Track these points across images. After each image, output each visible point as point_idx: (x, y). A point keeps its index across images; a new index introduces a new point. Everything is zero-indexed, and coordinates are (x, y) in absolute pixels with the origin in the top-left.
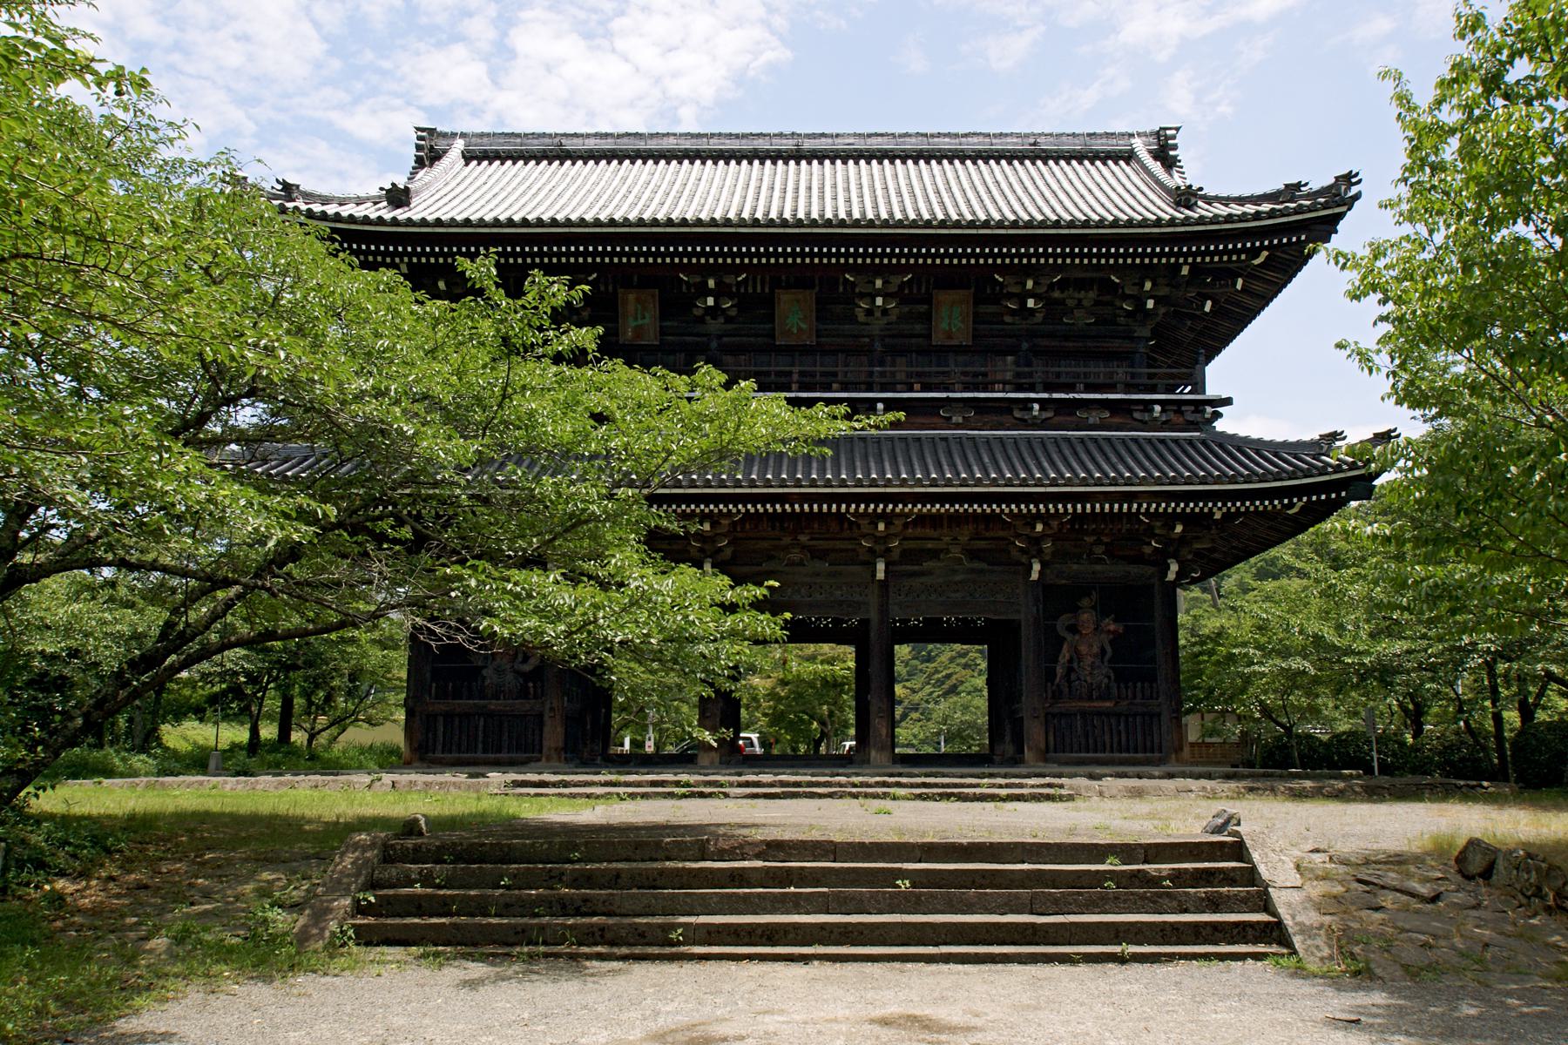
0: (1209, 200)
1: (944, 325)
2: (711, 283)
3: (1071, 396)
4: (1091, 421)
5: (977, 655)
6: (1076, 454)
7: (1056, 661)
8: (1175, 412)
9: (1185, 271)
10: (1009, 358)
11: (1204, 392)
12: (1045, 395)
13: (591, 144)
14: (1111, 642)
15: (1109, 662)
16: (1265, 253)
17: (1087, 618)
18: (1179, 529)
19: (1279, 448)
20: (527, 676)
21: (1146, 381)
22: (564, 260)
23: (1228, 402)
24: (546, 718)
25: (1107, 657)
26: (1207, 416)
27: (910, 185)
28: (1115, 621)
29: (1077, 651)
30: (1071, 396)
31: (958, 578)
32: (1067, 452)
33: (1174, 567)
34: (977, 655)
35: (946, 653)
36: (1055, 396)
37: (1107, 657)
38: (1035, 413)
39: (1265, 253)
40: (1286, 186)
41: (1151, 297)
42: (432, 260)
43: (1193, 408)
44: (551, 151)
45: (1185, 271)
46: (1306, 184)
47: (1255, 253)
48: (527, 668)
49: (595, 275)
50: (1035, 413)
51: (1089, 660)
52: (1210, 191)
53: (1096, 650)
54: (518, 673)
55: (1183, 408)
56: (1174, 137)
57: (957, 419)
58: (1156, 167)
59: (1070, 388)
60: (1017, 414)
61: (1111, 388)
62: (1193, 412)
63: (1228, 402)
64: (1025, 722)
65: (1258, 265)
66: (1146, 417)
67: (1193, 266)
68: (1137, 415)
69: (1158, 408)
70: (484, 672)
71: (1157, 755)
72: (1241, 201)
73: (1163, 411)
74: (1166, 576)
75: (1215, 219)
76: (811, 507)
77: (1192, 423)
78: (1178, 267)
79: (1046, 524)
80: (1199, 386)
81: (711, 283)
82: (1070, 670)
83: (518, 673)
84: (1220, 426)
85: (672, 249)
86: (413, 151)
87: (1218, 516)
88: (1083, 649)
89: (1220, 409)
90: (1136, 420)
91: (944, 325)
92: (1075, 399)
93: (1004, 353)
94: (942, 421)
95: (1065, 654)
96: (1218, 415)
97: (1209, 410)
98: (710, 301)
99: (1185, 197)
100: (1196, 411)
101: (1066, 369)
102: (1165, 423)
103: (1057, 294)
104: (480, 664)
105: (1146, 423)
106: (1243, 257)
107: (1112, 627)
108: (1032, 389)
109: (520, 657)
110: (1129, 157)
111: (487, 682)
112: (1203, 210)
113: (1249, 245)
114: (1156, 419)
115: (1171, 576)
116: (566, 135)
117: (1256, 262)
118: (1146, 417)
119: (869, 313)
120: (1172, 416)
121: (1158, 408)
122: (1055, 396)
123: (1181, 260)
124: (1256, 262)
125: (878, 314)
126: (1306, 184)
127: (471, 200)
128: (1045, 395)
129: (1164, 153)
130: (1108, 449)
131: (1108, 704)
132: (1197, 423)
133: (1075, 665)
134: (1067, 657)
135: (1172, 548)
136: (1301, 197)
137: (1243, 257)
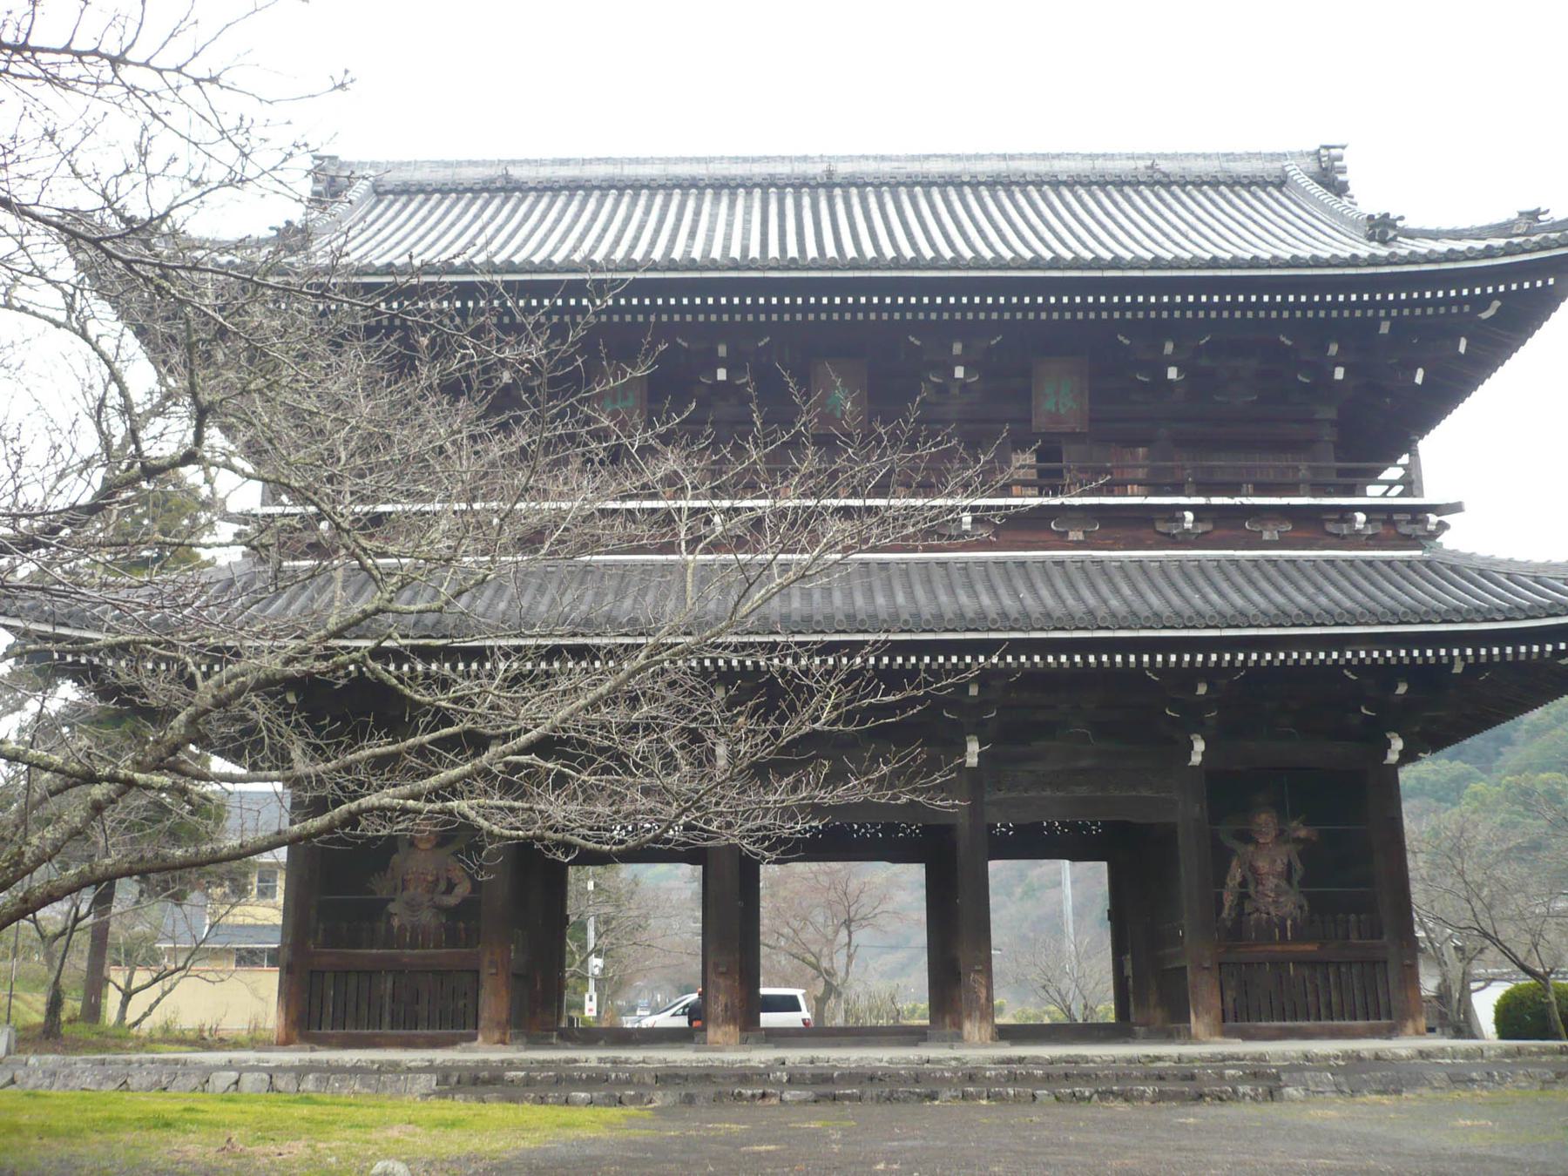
0: (1411, 234)
1: (1049, 405)
2: (722, 350)
3: (1237, 501)
4: (1266, 536)
5: (913, 875)
6: (1251, 582)
7: (1223, 884)
8: (1384, 522)
9: (1385, 328)
10: (1141, 450)
11: (1421, 495)
12: (1201, 500)
13: (546, 172)
14: (1300, 855)
15: (1303, 883)
16: (1497, 304)
17: (1265, 822)
18: (1402, 689)
19: (1513, 574)
20: (453, 913)
21: (1334, 479)
22: (823, 317)
23: (1456, 508)
24: (484, 976)
25: (1296, 878)
26: (1431, 527)
27: (1287, 208)
28: (1306, 824)
29: (1254, 870)
30: (1237, 501)
31: (1084, 763)
32: (1240, 580)
33: (1398, 744)
34: (913, 875)
35: (878, 873)
36: (1216, 501)
37: (1296, 878)
38: (1188, 525)
39: (1497, 304)
40: (1521, 214)
41: (1338, 365)
42: (640, 318)
43: (1409, 517)
44: (493, 181)
45: (1385, 328)
46: (1547, 211)
47: (1485, 301)
48: (451, 900)
49: (767, 340)
50: (1188, 525)
51: (1271, 882)
52: (1411, 223)
53: (1279, 867)
54: (441, 909)
55: (1395, 517)
56: (1340, 158)
57: (1076, 535)
58: (1328, 197)
59: (1233, 490)
60: (1161, 527)
61: (1293, 490)
62: (1409, 522)
63: (1456, 508)
64: (1190, 977)
65: (1485, 321)
66: (1345, 530)
67: (1396, 323)
68: (1330, 527)
69: (1361, 517)
70: (392, 908)
71: (1384, 1022)
72: (1457, 235)
73: (1196, 520)
74: (1385, 756)
75: (1412, 259)
76: (1085, 659)
77: (1408, 537)
78: (1376, 321)
79: (1211, 685)
80: (1410, 483)
81: (722, 350)
82: (1243, 897)
83: (441, 909)
84: (1447, 541)
85: (939, 300)
86: (818, 154)
87: (1458, 668)
88: (1263, 865)
89: (1445, 518)
90: (1331, 534)
91: (1049, 405)
92: (1243, 506)
93: (1133, 443)
94: (1056, 537)
95: (1236, 874)
96: (1443, 526)
97: (1433, 518)
98: (722, 374)
99: (1381, 228)
100: (1414, 521)
101: (1222, 463)
102: (1369, 537)
103: (1204, 362)
104: (384, 895)
105: (1344, 537)
106: (1467, 308)
107: (1302, 833)
108: (1178, 490)
109: (443, 886)
110: (1281, 183)
111: (396, 922)
112: (1404, 248)
113: (1502, 288)
114: (1358, 533)
115: (1393, 757)
116: (513, 162)
117: (1485, 315)
118: (1345, 530)
119: (941, 389)
120: (1380, 529)
121: (1189, 516)
122: (1216, 501)
123: (1382, 313)
124: (1485, 315)
125: (955, 391)
126: (1547, 211)
127: (386, 246)
128: (1201, 500)
129: (1330, 178)
130: (1256, 575)
131: (1309, 947)
132: (1417, 537)
133: (1251, 890)
134: (1238, 878)
135: (1396, 715)
136: (1543, 229)
137: (1467, 308)
